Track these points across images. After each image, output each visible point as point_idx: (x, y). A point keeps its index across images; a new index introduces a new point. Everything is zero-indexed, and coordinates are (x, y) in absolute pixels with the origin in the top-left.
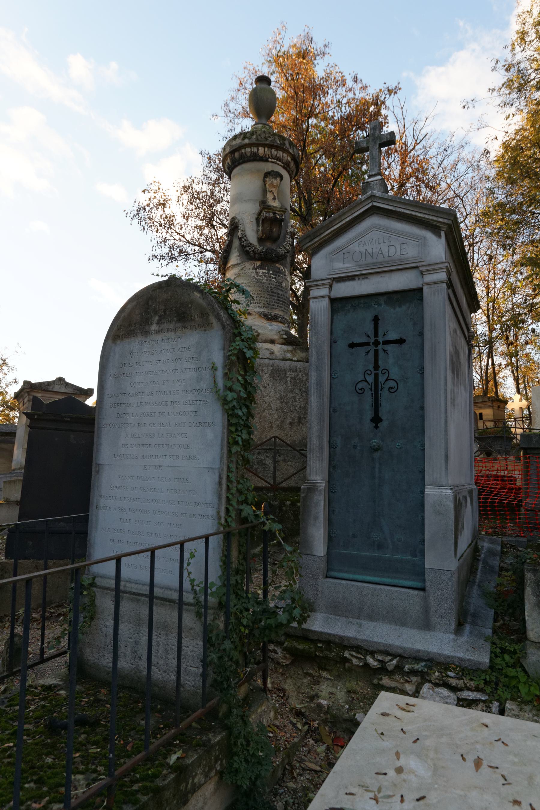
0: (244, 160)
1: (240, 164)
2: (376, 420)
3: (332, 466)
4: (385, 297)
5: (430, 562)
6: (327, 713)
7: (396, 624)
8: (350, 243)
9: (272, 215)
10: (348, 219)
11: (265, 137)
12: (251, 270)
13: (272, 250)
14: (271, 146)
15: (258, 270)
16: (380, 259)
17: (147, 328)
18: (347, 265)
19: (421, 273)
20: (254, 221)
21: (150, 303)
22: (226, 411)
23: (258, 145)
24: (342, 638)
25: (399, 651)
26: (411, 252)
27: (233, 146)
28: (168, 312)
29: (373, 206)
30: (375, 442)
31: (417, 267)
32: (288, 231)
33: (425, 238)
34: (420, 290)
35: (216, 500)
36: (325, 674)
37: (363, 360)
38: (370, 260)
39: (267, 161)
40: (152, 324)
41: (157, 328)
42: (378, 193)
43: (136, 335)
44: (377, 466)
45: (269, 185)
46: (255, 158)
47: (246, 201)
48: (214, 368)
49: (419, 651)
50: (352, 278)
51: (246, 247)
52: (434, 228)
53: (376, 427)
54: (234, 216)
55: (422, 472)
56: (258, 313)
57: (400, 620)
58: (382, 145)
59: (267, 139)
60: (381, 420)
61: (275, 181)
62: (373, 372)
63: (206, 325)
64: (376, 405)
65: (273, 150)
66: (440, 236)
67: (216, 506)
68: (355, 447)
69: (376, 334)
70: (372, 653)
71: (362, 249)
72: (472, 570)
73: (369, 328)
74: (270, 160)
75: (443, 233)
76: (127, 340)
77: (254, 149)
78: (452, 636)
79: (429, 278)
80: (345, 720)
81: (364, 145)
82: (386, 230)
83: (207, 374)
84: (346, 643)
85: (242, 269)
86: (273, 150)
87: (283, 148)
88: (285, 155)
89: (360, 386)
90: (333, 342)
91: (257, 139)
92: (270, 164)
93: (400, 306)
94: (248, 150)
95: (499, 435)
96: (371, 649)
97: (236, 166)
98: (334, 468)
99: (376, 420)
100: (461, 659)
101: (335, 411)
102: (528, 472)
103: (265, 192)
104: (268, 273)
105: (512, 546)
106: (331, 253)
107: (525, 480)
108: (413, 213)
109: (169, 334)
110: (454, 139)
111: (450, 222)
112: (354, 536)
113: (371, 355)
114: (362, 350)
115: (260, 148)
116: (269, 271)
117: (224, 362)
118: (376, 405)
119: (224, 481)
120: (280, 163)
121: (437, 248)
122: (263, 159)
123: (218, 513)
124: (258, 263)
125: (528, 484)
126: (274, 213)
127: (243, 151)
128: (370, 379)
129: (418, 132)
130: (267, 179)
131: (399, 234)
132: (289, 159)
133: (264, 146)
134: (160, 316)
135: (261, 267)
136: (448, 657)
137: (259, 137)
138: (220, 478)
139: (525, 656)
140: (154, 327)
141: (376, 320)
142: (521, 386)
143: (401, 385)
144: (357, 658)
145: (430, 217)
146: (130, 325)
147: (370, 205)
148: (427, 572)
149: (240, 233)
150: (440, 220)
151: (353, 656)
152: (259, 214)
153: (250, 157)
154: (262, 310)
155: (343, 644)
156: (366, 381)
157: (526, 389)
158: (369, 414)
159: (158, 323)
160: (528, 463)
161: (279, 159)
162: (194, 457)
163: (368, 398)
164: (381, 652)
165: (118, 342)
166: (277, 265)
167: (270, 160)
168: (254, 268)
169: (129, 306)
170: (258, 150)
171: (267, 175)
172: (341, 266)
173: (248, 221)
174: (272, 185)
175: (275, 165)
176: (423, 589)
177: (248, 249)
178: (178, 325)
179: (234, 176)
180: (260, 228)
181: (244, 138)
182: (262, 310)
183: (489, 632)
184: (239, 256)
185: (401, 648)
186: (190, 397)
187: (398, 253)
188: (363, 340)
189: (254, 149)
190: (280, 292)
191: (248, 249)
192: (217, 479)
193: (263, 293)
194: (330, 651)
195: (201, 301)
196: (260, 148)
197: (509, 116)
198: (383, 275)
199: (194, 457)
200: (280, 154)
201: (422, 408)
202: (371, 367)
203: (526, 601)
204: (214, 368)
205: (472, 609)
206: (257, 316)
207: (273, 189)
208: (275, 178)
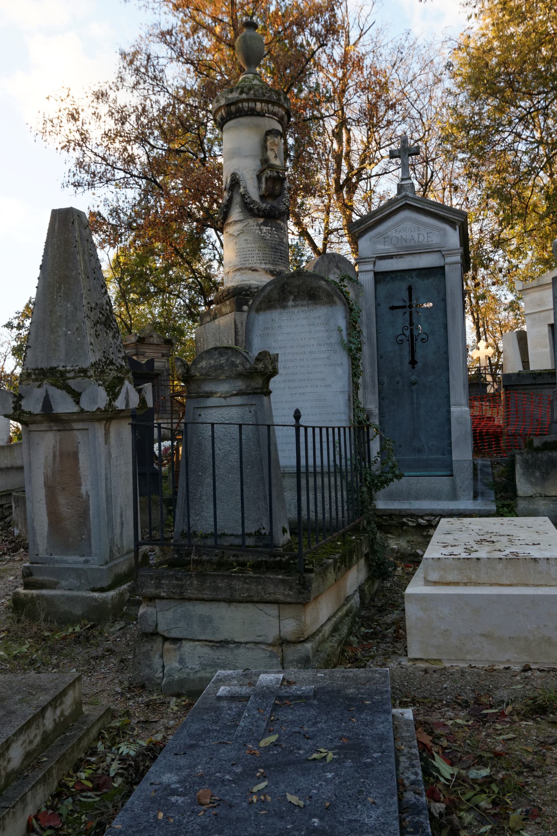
0: (241, 114)
1: (236, 117)
2: (413, 362)
3: (381, 398)
4: (416, 272)
5: (456, 456)
6: (398, 552)
7: (434, 499)
8: (389, 229)
9: (275, 174)
10: (388, 212)
11: (263, 93)
12: (255, 227)
13: (275, 207)
14: (268, 102)
15: (262, 227)
16: (413, 243)
17: (285, 303)
18: (387, 247)
19: (443, 256)
20: (255, 177)
21: (286, 286)
22: (349, 355)
23: (255, 101)
24: (400, 510)
25: (440, 512)
26: (435, 240)
27: (229, 99)
28: (301, 293)
29: (406, 204)
30: (414, 378)
31: (440, 251)
32: (286, 186)
33: (445, 230)
34: (443, 268)
35: (347, 410)
36: (389, 535)
37: (401, 319)
38: (404, 244)
39: (264, 116)
40: (289, 301)
41: (293, 304)
42: (411, 195)
43: (276, 308)
44: (415, 395)
45: (271, 143)
46: (253, 113)
47: (246, 156)
48: (340, 330)
49: (452, 510)
50: (391, 257)
51: (249, 204)
52: (452, 223)
53: (413, 368)
54: (232, 171)
55: (448, 397)
56: (264, 269)
57: (436, 496)
58: (411, 155)
59: (264, 95)
60: (416, 363)
61: (276, 140)
62: (409, 328)
63: (331, 302)
64: (413, 352)
65: (270, 106)
66: (455, 229)
67: (347, 413)
68: (398, 383)
69: (410, 300)
70: (422, 517)
71: (398, 235)
72: (475, 475)
73: (405, 294)
74: (267, 115)
75: (457, 227)
76: (268, 312)
77: (252, 105)
78: (471, 501)
79: (449, 260)
80: (410, 555)
81: (397, 154)
82: (416, 221)
83: (335, 334)
84: (403, 513)
85: (246, 226)
86: (270, 106)
87: (279, 104)
88: (280, 110)
89: (400, 338)
90: (378, 305)
91: (255, 95)
92: (267, 119)
93: (428, 279)
94: (246, 104)
95: (474, 381)
96: (421, 514)
97: (231, 119)
98: (383, 399)
99: (413, 362)
100: (480, 510)
101: (381, 357)
102: (509, 405)
103: (264, 148)
104: (271, 230)
105: (498, 463)
106: (374, 237)
107: (506, 412)
108: (437, 211)
109: (303, 308)
110: (409, 37)
111: (463, 220)
112: (400, 446)
113: (407, 315)
114: (400, 312)
115: (258, 103)
116: (272, 228)
117: (347, 326)
118: (413, 352)
119: (352, 398)
120: (276, 118)
121: (453, 238)
122: (261, 114)
123: (349, 417)
124: (261, 220)
125: (508, 415)
126: (278, 172)
127: (241, 106)
128: (407, 333)
129: (364, 20)
130: (269, 137)
131: (426, 225)
132: (284, 113)
133: (262, 101)
134: (295, 296)
135: (264, 224)
136: (471, 510)
137: (257, 93)
138: (349, 397)
139: (516, 506)
140: (290, 303)
141: (410, 289)
142: (481, 330)
143: (430, 337)
144: (411, 521)
145: (449, 216)
146: (270, 301)
147: (404, 202)
148: (454, 463)
149: (242, 190)
150: (456, 218)
151: (409, 520)
152: (262, 172)
153: (248, 111)
154: (268, 266)
155: (401, 514)
156: (404, 334)
157: (485, 334)
158: (408, 359)
159: (293, 300)
160: (508, 397)
161: (275, 114)
162: (330, 386)
163: (406, 347)
164: (427, 515)
165: (261, 313)
166: (279, 222)
167: (267, 115)
168: (258, 225)
169: (50, 249)
170: (256, 105)
171: (269, 133)
172: (383, 248)
173: (249, 177)
174: (273, 143)
175: (271, 120)
176: (452, 476)
177: (252, 206)
178: (310, 302)
179: (229, 128)
180: (264, 185)
181: (242, 92)
182: (268, 266)
183: (494, 499)
184: (241, 212)
185: (441, 510)
186: (323, 348)
187: (426, 239)
188: (401, 304)
189: (252, 105)
190: (282, 248)
191: (252, 206)
192: (347, 398)
193: (267, 249)
194: (392, 520)
195: (326, 287)
196: (258, 103)
197: (471, 15)
198: (414, 255)
199: (330, 386)
200: (276, 109)
201: (446, 353)
202: (407, 324)
203: (517, 473)
204: (340, 330)
205: (480, 491)
206: (264, 272)
207: (275, 148)
208: (277, 137)
